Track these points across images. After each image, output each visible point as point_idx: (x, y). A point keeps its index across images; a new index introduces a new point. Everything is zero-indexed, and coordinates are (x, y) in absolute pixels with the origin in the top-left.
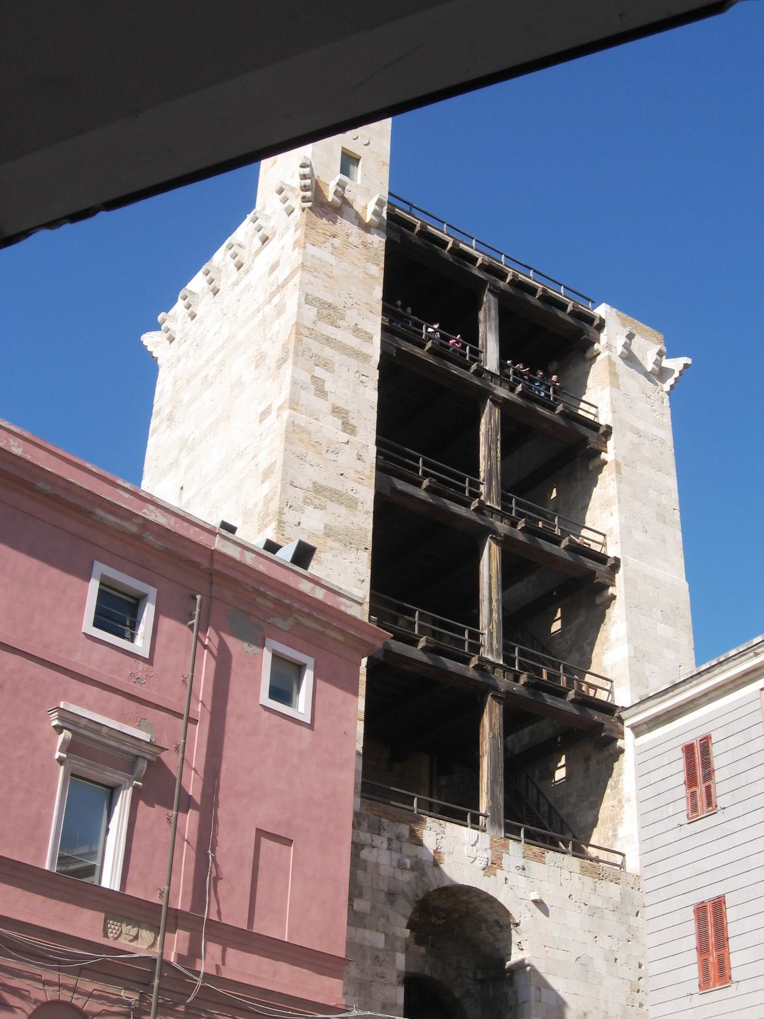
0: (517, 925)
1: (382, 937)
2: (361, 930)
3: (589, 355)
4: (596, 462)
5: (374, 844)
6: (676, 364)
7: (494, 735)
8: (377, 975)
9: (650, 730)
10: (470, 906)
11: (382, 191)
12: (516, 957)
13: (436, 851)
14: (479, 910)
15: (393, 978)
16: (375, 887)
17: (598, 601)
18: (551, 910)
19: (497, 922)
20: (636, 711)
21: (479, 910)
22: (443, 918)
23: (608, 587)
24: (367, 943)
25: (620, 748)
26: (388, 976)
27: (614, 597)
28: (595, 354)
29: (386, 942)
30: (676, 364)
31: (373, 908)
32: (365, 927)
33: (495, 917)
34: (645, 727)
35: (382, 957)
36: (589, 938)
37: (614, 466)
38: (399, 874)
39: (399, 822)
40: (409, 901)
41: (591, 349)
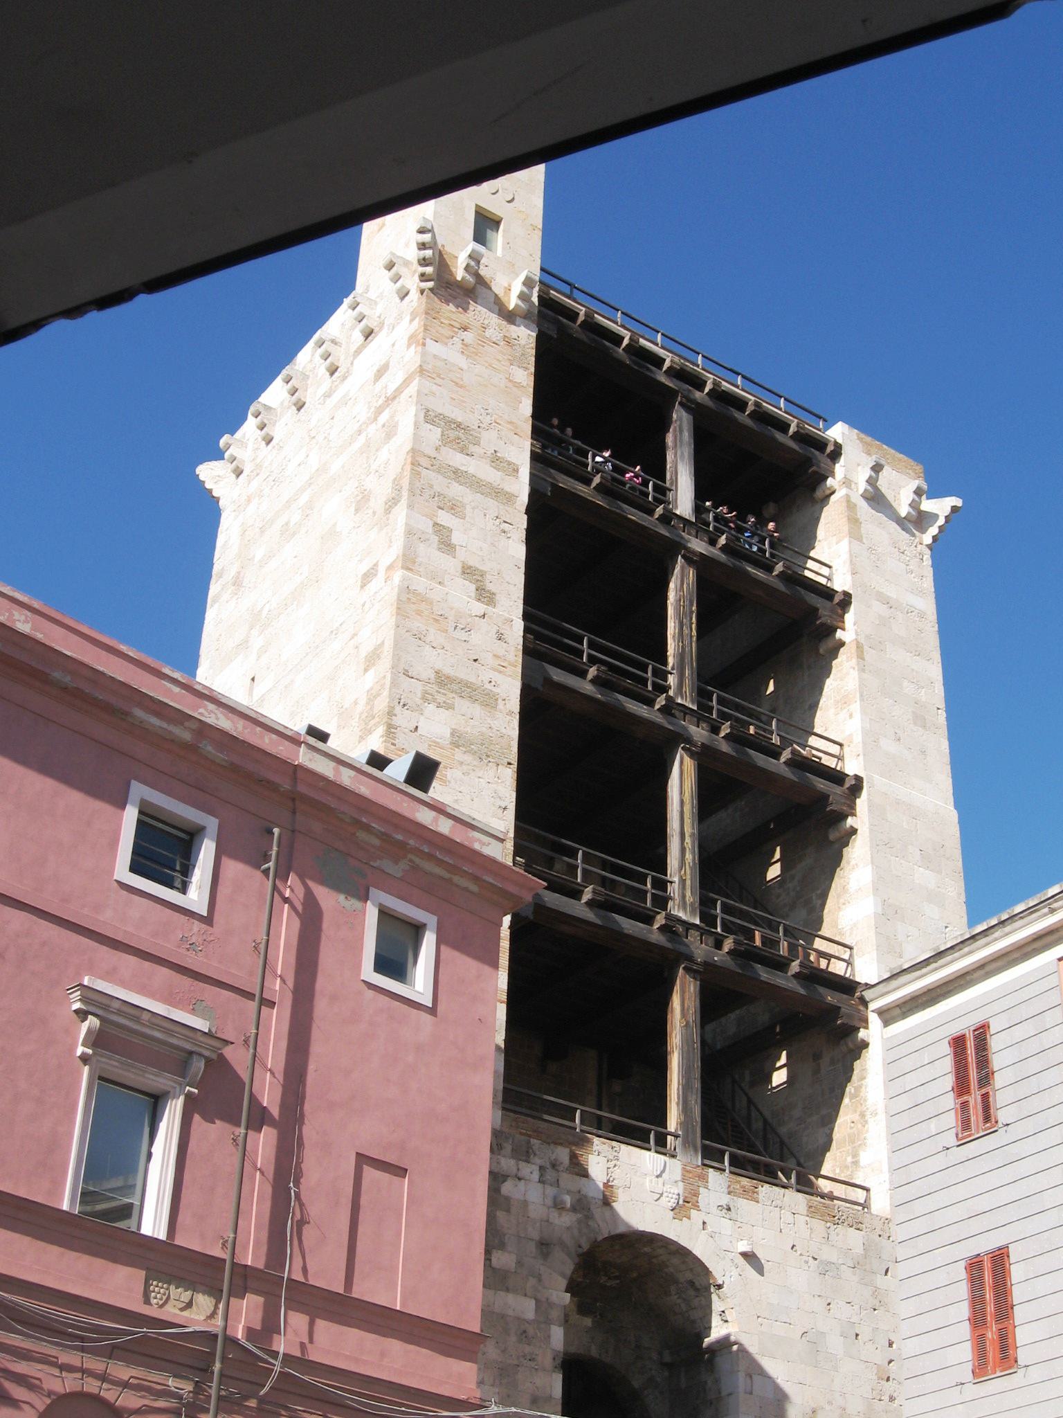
0: (719, 1287)
1: (532, 1304)
3: (819, 494)
4: (829, 643)
6: (941, 507)
7: (687, 1023)
8: (524, 1356)
9: (904, 1015)
12: (717, 1331)
13: (606, 1185)
14: (667, 1266)
15: (547, 1360)
17: (833, 836)
18: (767, 1266)
19: (691, 1283)
20: (885, 990)
21: (667, 1266)
22: (616, 1278)
23: (846, 817)
24: (510, 1312)
25: (863, 1041)
26: (539, 1358)
27: (854, 831)
28: (828, 492)
30: (941, 507)
31: (519, 1263)
32: (508, 1290)
33: (689, 1276)
34: (898, 1011)
35: (531, 1331)
36: (819, 1305)
38: (555, 1217)
39: (555, 1143)
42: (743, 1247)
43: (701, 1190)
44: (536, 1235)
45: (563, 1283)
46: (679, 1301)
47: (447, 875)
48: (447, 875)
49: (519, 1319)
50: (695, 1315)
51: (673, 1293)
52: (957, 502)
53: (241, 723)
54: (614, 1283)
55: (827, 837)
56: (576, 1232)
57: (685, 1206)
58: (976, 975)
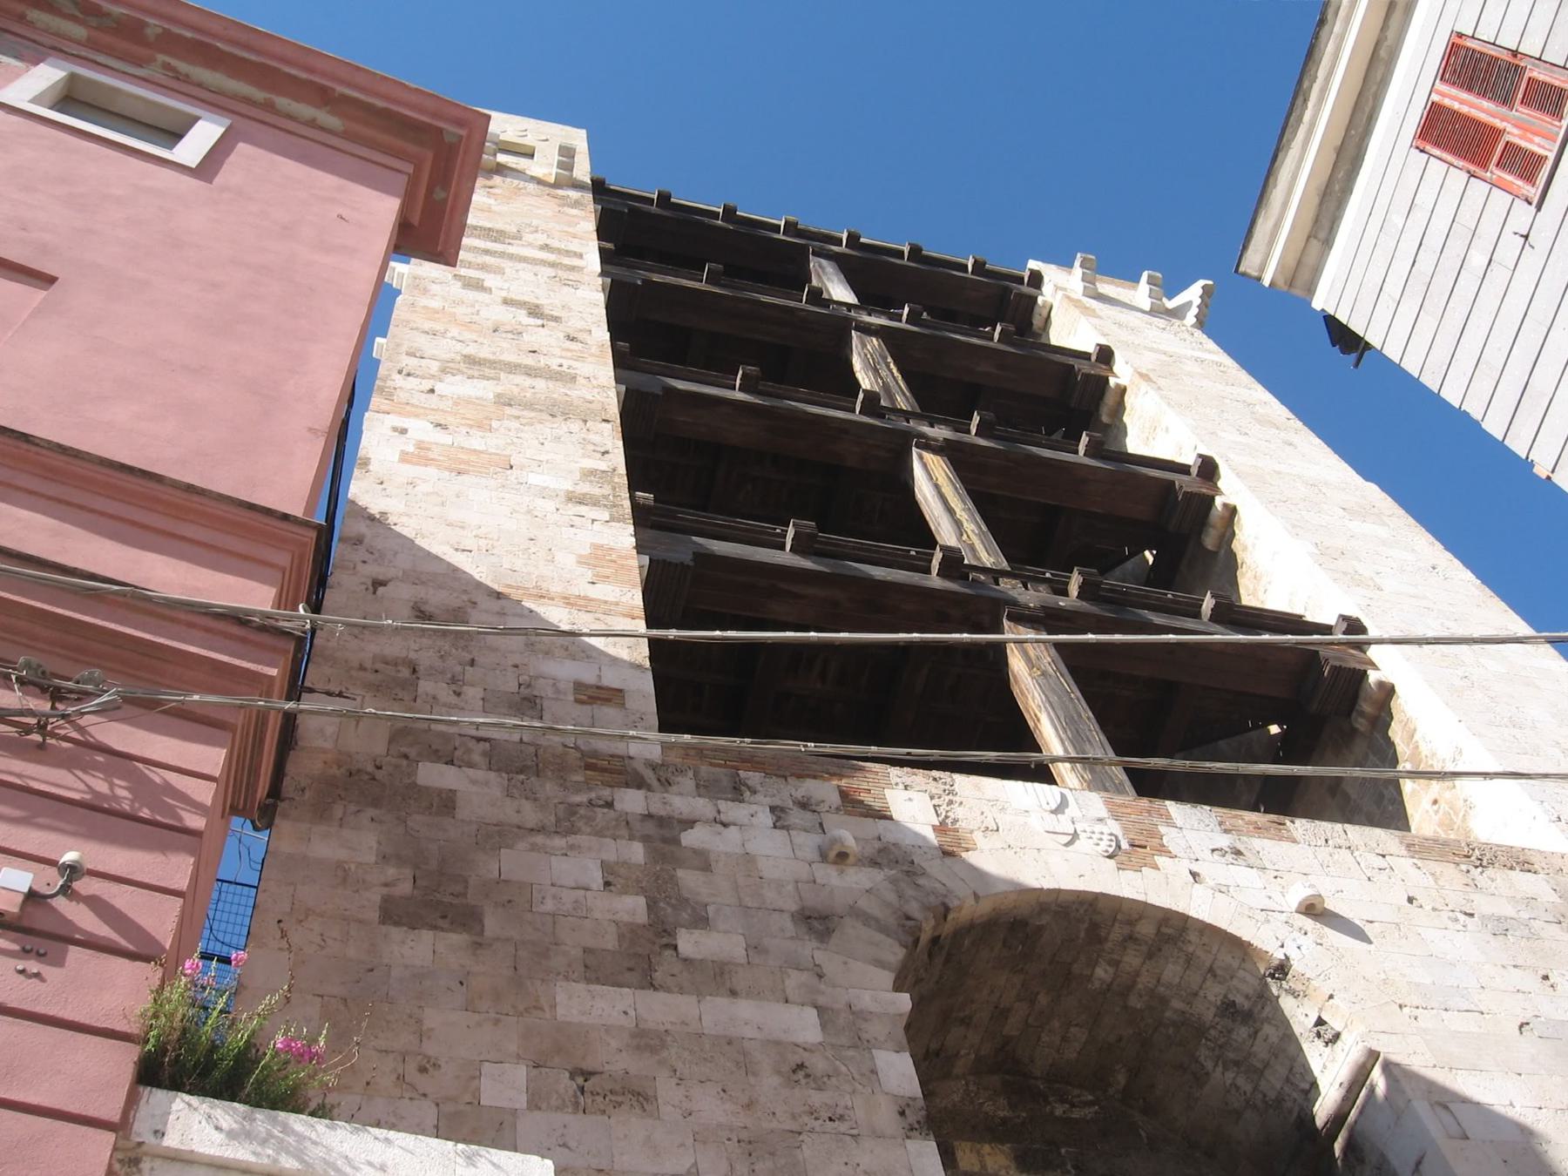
0: (1282, 970)
1: (811, 1015)
2: (722, 1001)
3: (1037, 322)
4: (1109, 400)
5: (723, 818)
6: (1193, 294)
7: (1044, 674)
8: (811, 1112)
9: (1328, 243)
10: (1135, 1002)
11: (588, 168)
12: (1330, 1074)
13: (941, 829)
14: (1164, 1001)
15: (886, 1118)
16: (748, 902)
17: (1210, 541)
18: (1368, 929)
19: (1228, 1008)
20: (1271, 223)
21: (1164, 1001)
22: (1091, 1104)
23: (1213, 499)
24: (749, 1032)
25: (1381, 684)
26: (860, 1114)
27: (1232, 511)
28: (1045, 313)
29: (823, 1026)
30: (1193, 294)
31: (754, 948)
32: (733, 993)
33: (1214, 992)
34: (1315, 245)
35: (818, 1064)
36: (1532, 983)
37: (1137, 379)
38: (829, 875)
39: (799, 777)
40: (883, 929)
41: (1036, 310)
42: (1298, 894)
43: (1163, 829)
44: (793, 906)
45: (887, 978)
46: (1230, 1075)
47: (259, 95)
48: (259, 95)
49: (778, 1043)
50: (1273, 1081)
51: (1209, 1065)
52: (1202, 282)
53: (189, 534)
54: (1089, 1112)
55: (1203, 548)
56: (891, 897)
57: (1137, 850)
58: (1391, 34)
